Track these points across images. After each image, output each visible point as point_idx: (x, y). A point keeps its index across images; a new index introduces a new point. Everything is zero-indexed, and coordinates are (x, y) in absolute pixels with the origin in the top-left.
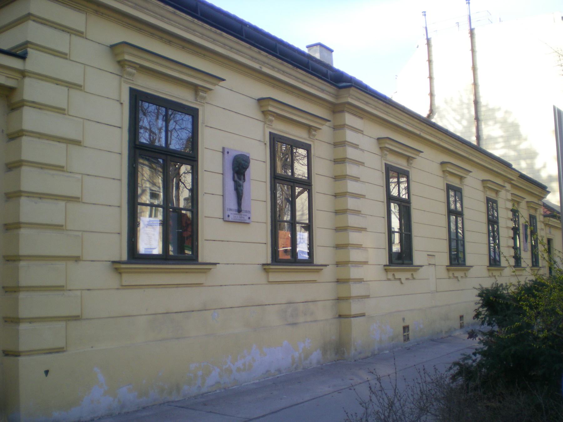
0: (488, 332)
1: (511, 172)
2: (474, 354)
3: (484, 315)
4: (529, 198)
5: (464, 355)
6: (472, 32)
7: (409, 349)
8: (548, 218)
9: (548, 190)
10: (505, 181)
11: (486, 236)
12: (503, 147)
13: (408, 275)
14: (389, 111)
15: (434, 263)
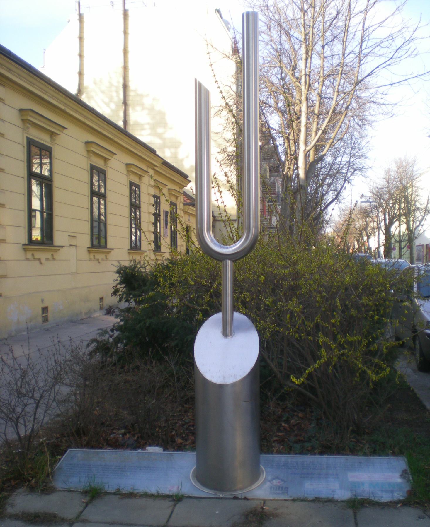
0: (125, 308)
1: (155, 158)
2: (112, 330)
3: (121, 291)
4: (170, 186)
5: (101, 329)
6: (125, 14)
7: (48, 330)
8: (188, 206)
9: (189, 179)
10: (148, 167)
11: (128, 221)
12: (150, 134)
13: (48, 255)
14: (34, 82)
15: (75, 244)
